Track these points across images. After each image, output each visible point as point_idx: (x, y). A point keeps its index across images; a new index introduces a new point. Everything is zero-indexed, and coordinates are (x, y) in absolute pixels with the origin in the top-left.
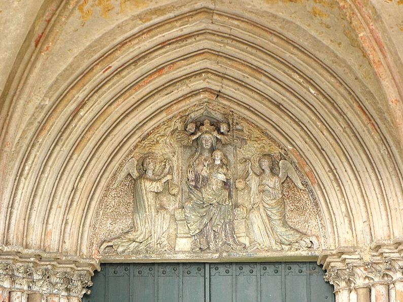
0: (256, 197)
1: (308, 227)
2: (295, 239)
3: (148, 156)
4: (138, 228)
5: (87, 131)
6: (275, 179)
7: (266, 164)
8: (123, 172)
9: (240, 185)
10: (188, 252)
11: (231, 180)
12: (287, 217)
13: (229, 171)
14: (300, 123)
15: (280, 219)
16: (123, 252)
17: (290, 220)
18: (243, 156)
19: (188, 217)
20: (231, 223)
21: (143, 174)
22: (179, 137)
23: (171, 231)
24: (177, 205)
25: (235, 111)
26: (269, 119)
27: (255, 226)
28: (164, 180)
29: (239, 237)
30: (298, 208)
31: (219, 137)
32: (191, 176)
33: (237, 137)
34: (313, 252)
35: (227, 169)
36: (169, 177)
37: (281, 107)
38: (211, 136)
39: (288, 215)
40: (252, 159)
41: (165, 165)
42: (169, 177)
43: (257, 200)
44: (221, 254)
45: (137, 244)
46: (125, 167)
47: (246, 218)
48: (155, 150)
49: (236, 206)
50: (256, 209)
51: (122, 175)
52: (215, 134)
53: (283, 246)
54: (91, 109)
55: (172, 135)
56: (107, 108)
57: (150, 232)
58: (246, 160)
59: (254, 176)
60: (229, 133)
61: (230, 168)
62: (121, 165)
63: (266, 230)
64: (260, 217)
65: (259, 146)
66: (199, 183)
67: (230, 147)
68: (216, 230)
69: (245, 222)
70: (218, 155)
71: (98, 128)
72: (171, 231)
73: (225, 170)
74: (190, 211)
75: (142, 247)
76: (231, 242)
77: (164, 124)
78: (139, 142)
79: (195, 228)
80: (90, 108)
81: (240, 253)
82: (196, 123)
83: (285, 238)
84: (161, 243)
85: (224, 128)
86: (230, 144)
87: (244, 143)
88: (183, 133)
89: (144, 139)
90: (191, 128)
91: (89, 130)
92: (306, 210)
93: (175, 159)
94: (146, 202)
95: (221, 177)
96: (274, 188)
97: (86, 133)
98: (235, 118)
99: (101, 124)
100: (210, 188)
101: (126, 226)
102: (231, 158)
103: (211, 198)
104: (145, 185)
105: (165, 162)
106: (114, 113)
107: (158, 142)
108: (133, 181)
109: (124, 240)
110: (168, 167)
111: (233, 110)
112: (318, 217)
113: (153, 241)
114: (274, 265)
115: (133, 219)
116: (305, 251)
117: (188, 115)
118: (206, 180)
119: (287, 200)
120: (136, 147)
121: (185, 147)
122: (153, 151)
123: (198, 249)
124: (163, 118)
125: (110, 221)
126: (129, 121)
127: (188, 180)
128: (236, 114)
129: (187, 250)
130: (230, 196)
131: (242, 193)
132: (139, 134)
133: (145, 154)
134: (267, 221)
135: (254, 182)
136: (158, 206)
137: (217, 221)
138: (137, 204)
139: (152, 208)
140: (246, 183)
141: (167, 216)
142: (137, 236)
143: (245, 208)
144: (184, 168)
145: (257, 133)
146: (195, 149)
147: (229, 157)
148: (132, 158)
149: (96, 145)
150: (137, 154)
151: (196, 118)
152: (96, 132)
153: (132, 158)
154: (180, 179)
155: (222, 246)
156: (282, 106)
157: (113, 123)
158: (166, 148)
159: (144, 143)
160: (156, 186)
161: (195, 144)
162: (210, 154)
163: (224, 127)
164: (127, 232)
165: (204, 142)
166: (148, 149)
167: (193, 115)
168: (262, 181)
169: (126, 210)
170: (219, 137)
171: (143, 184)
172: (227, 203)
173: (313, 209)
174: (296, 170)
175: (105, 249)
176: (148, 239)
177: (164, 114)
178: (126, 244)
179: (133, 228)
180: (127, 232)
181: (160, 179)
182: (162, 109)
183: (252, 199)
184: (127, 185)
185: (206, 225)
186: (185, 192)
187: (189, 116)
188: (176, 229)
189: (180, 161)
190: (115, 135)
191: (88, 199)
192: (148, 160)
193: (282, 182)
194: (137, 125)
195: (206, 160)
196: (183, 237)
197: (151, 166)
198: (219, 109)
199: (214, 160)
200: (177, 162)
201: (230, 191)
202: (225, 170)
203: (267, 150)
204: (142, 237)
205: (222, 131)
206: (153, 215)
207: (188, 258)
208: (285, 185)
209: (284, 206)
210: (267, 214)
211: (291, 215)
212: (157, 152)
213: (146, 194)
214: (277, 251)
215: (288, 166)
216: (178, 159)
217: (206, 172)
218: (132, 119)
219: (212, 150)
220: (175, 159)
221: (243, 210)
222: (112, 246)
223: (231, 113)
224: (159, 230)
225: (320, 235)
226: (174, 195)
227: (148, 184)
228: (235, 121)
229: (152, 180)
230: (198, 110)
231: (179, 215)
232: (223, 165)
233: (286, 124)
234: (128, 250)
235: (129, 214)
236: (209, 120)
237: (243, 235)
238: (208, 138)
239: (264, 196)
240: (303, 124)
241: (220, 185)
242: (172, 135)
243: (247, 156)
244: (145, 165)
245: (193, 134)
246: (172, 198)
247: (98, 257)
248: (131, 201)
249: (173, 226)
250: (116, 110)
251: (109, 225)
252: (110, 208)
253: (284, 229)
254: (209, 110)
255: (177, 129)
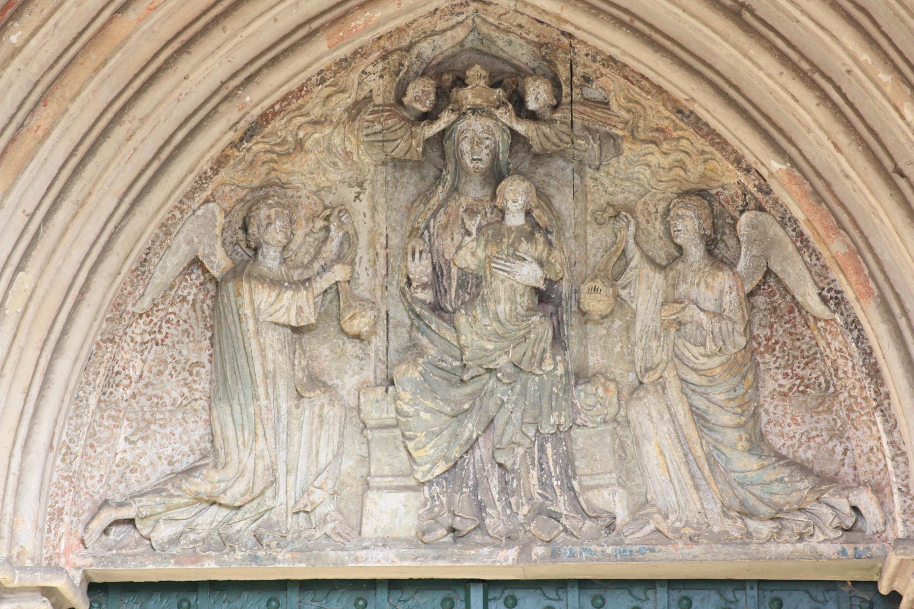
0: (654, 344)
1: (845, 453)
2: (795, 496)
3: (266, 197)
4: (226, 454)
5: (37, 104)
6: (724, 279)
7: (689, 227)
8: (175, 253)
9: (596, 304)
10: (409, 542)
11: (564, 283)
12: (764, 418)
13: (556, 253)
14: (817, 77)
15: (739, 426)
16: (174, 541)
17: (778, 429)
18: (607, 198)
19: (407, 416)
20: (561, 436)
21: (247, 249)
22: (378, 127)
23: (348, 464)
24: (368, 374)
25: (578, 34)
26: (703, 62)
27: (650, 450)
28: (322, 284)
29: (591, 488)
30: (803, 387)
31: (521, 127)
32: (420, 269)
33: (588, 129)
34: (861, 547)
35: (550, 243)
36: (339, 273)
37: (747, 16)
38: (490, 123)
39: (771, 409)
40: (640, 207)
41: (327, 229)
42: (339, 273)
43: (659, 355)
44: (525, 550)
45: (225, 512)
46: (181, 236)
47: (620, 422)
48: (292, 173)
49: (580, 376)
50: (651, 388)
51: (171, 263)
52: (506, 116)
53: (752, 524)
54: (51, 22)
55: (352, 119)
56: (110, 20)
57: (272, 469)
58: (617, 212)
59: (647, 270)
60: (557, 116)
61: (559, 239)
62: (167, 229)
63: (687, 463)
64: (667, 416)
65: (666, 162)
66: (447, 296)
67: (561, 163)
68: (509, 464)
69: (614, 433)
70: (515, 195)
71: (78, 94)
72: (348, 464)
73: (540, 247)
74: (414, 394)
75: (242, 525)
76: (562, 505)
77: (323, 81)
78: (234, 145)
79: (431, 456)
80: (48, 18)
81: (593, 547)
82: (438, 76)
83: (758, 492)
84: (308, 509)
85: (537, 95)
86: (562, 154)
87: (612, 150)
88: (393, 115)
89: (249, 134)
90: (420, 95)
91: (43, 100)
92: (836, 394)
93: (363, 206)
94: (257, 364)
95: (529, 274)
96: (718, 314)
97: (32, 111)
98: (581, 59)
99: (91, 78)
100: (486, 311)
101: (186, 449)
102: (564, 202)
103: (490, 346)
104: (252, 301)
105: (327, 218)
106: (135, 37)
107: (300, 145)
108: (211, 286)
109: (176, 501)
110: (336, 235)
111: (569, 29)
112: (879, 420)
113: (281, 501)
114: (719, 592)
115: (209, 422)
116: (832, 541)
117: (409, 49)
118: (473, 285)
119: (767, 356)
120: (220, 163)
121: (399, 163)
122: (284, 178)
123: (442, 532)
124: (318, 59)
125: (125, 430)
126: (193, 69)
127: (409, 282)
128: (584, 43)
129: (403, 535)
130: (559, 340)
131: (604, 332)
132: (230, 114)
133: (253, 190)
134: (691, 432)
135: (646, 291)
136: (300, 375)
137: (510, 429)
138: (223, 367)
139: (281, 382)
140: (617, 296)
141: (333, 413)
142: (223, 485)
143: (612, 386)
144: (395, 241)
145: (658, 114)
146: (432, 172)
147: (557, 202)
148: (207, 201)
149: (72, 154)
150: (227, 189)
151: (440, 58)
152: (74, 108)
153: (207, 201)
154: (379, 280)
155: (530, 518)
156: (752, 12)
157: (137, 76)
158: (335, 164)
159: (249, 149)
160: (294, 306)
161: (434, 155)
162: (488, 191)
163: (541, 91)
164: (189, 472)
165: (465, 146)
166: (264, 169)
167: (426, 48)
168: (675, 286)
169: (185, 390)
170: (521, 127)
171: (247, 297)
172: (548, 366)
173: (863, 388)
174: (799, 250)
175: (106, 532)
176: (262, 493)
177: (321, 45)
178: (183, 514)
179: (210, 454)
180: (189, 472)
181: (309, 279)
182: (315, 25)
183: (639, 353)
184: (190, 298)
185: (472, 445)
186: (399, 325)
187: (415, 51)
188: (366, 460)
189: (380, 217)
190: (142, 121)
191: (42, 349)
192: (264, 212)
193: (748, 288)
194: (223, 83)
195: (471, 212)
196: (389, 489)
197: (275, 235)
198: (520, 26)
199: (502, 212)
200: (374, 217)
201: (560, 322)
202: (540, 247)
203: (694, 172)
204: (240, 487)
205: (532, 105)
206: (284, 407)
207: (406, 563)
208: (760, 300)
209: (756, 377)
210: (691, 405)
211: (780, 412)
212: (296, 180)
213: (257, 332)
214: (723, 539)
215: (771, 233)
216: (374, 209)
217: (473, 254)
218: (204, 60)
219: (495, 176)
220: (363, 206)
221: (606, 390)
222: (131, 521)
223: (565, 41)
224: (302, 463)
225: (888, 484)
226: (358, 337)
227: (264, 296)
228: (579, 71)
229: (276, 283)
230: (445, 31)
231: (377, 409)
232: (533, 229)
233: (766, 79)
234: (192, 536)
235: (196, 405)
236: (484, 67)
237: (604, 480)
238: (479, 134)
239: (679, 342)
240: (829, 80)
241: (525, 301)
242: (352, 119)
243: (621, 196)
244: (252, 229)
245: (429, 117)
246: (351, 347)
247: (79, 562)
248: (205, 358)
249: (354, 447)
250: (145, 27)
251: (122, 444)
252: (127, 382)
253: (753, 463)
254: (484, 29)
255: (368, 99)
